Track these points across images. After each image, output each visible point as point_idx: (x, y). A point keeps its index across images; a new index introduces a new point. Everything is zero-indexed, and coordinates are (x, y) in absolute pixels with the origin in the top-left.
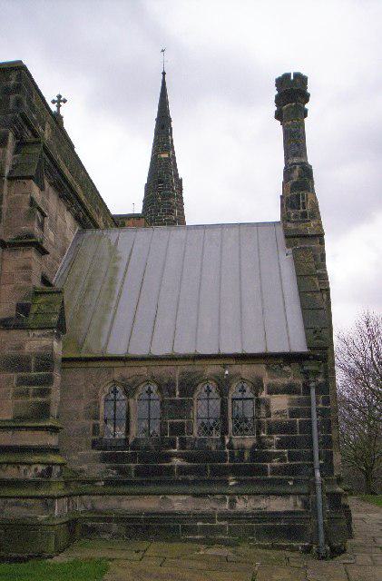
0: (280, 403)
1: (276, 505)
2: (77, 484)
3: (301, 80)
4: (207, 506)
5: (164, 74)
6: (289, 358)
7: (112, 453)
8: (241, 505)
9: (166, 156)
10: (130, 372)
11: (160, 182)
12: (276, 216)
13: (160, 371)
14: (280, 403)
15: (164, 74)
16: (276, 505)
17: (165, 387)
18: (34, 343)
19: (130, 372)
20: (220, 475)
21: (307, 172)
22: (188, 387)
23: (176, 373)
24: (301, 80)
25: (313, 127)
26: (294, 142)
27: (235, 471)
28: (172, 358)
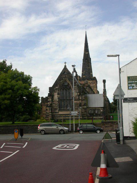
0: (102, 110)
1: (101, 117)
2: (88, 116)
3: (105, 80)
4: (97, 117)
5: (86, 32)
6: (102, 107)
7: (90, 114)
8: (99, 117)
9: (87, 53)
10: (91, 108)
11: (86, 59)
12: (103, 93)
13: (93, 108)
14: (102, 110)
15: (86, 32)
16: (101, 117)
17: (94, 109)
18: (85, 107)
19: (91, 108)
20: (97, 115)
21: (105, 90)
22: (95, 109)
23: (94, 108)
24: (105, 80)
25: (106, 83)
26: (104, 86)
27: (99, 115)
28: (94, 107)
